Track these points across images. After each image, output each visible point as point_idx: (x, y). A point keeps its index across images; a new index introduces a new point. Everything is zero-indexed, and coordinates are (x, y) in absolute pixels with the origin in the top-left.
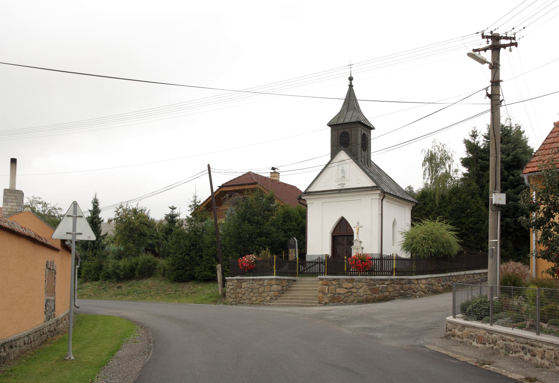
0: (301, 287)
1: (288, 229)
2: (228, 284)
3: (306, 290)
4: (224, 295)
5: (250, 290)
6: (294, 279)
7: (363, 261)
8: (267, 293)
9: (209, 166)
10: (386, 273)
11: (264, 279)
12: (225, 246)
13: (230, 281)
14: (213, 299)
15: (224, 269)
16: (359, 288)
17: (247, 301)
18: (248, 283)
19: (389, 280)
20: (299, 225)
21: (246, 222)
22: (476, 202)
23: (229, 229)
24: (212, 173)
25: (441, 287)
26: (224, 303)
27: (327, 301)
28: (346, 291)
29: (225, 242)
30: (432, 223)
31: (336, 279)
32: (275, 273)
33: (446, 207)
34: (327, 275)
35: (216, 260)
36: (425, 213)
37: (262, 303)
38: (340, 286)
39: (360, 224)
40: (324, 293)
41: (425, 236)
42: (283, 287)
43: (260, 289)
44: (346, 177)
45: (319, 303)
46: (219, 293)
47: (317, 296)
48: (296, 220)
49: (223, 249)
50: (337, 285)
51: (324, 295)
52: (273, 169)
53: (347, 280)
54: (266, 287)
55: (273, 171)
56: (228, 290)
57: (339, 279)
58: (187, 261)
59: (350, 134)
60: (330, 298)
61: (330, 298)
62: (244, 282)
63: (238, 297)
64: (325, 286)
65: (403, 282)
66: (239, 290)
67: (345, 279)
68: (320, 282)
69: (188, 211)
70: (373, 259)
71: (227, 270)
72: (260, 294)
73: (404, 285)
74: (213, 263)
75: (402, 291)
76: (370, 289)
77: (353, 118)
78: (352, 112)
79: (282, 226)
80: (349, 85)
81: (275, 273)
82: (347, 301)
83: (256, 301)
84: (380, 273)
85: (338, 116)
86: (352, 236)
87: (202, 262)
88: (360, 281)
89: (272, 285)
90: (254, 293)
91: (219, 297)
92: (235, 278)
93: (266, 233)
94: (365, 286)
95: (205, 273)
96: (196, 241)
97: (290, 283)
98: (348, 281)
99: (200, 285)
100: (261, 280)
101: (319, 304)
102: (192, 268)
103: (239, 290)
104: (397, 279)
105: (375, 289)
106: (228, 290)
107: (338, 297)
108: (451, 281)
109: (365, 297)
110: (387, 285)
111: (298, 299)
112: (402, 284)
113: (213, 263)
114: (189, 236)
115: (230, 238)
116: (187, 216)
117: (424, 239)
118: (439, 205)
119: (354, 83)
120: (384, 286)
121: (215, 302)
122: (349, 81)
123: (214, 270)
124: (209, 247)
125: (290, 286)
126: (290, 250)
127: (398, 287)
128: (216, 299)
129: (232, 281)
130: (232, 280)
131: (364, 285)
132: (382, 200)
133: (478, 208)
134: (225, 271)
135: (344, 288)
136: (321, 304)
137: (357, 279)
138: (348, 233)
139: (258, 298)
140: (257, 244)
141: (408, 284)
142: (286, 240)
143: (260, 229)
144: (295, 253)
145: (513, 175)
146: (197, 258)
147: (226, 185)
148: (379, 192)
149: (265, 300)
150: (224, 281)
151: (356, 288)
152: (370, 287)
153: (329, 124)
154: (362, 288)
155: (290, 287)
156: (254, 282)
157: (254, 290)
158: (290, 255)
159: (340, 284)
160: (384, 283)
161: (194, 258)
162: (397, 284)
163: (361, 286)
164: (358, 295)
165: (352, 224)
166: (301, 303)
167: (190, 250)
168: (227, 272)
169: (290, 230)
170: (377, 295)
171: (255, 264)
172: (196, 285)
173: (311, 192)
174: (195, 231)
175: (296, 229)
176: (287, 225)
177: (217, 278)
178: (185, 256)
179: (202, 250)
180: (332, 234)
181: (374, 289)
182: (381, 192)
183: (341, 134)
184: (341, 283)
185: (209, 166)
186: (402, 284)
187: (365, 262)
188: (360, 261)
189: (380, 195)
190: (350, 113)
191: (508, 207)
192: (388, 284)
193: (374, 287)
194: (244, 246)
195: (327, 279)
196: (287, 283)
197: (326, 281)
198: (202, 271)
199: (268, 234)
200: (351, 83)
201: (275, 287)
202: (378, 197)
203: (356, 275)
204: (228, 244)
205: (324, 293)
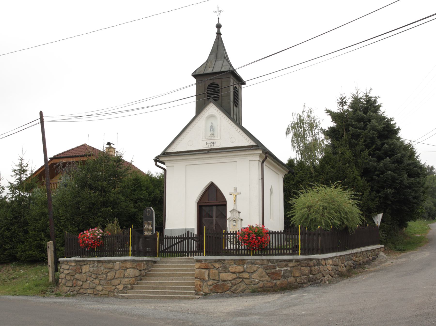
0: (165, 271)
1: (138, 199)
2: (62, 267)
3: (173, 275)
4: (56, 282)
5: (93, 276)
6: (154, 260)
8: (120, 279)
9: (41, 113)
11: (115, 261)
12: (58, 219)
13: (66, 263)
14: (40, 288)
15: (57, 247)
16: (252, 273)
17: (89, 291)
18: (91, 266)
19: (294, 261)
20: (150, 195)
21: (87, 189)
22: (352, 171)
23: (64, 198)
24: (45, 123)
25: (345, 269)
26: (56, 294)
27: (207, 290)
28: (234, 276)
29: (59, 213)
31: (219, 260)
32: (130, 253)
33: (317, 177)
34: (207, 254)
35: (46, 236)
36: (294, 183)
37: (112, 293)
38: (226, 270)
39: (238, 191)
41: (325, 204)
42: (140, 271)
43: (109, 274)
44: (216, 134)
45: (197, 294)
46: (48, 280)
47: (193, 284)
48: (147, 188)
49: (56, 222)
50: (221, 269)
51: (204, 283)
52: (109, 144)
53: (235, 261)
54: (118, 272)
55: (108, 146)
56: (62, 276)
57: (224, 260)
58: (7, 237)
61: (211, 287)
62: (85, 265)
63: (77, 285)
64: (204, 270)
65: (311, 263)
66: (77, 276)
67: (232, 260)
68: (198, 265)
69: (12, 176)
71: (59, 248)
72: (109, 282)
73: (313, 268)
74: (41, 240)
75: (311, 276)
78: (222, 61)
79: (131, 195)
80: (216, 33)
81: (130, 253)
82: (236, 290)
83: (102, 290)
84: (278, 252)
85: (205, 65)
86: (224, 205)
87: (27, 238)
88: (253, 263)
90: (100, 280)
91: (48, 285)
92: (72, 259)
93: (112, 202)
94: (260, 270)
95: (30, 252)
96: (20, 213)
97: (150, 266)
98: (237, 263)
99: (23, 268)
100: (110, 261)
102: (14, 246)
103: (77, 276)
104: (305, 259)
105: (275, 273)
106: (62, 276)
107: (223, 284)
108: (351, 260)
109: (261, 284)
110: (291, 267)
112: (310, 266)
113: (41, 240)
114: (11, 206)
115: (66, 208)
116: (10, 183)
117: (325, 208)
119: (222, 30)
120: (287, 269)
121: (43, 293)
123: (42, 249)
124: (37, 220)
125: (150, 269)
126: (146, 223)
127: (306, 270)
128: (45, 288)
129: (69, 264)
130: (68, 262)
131: (259, 268)
133: (355, 177)
134: (58, 250)
135: (231, 272)
136: (198, 295)
137: (249, 260)
138: (219, 202)
139: (105, 286)
140: (100, 216)
142: (136, 212)
143: (104, 197)
144: (152, 226)
145: (387, 143)
146: (20, 234)
147: (58, 156)
149: (116, 290)
150: (57, 263)
152: (268, 271)
153: (194, 74)
154: (257, 273)
155: (149, 271)
156: (100, 265)
157: (101, 276)
158: (145, 229)
159: (225, 267)
160: (288, 265)
161: (17, 234)
162: (305, 266)
163: (255, 269)
165: (226, 191)
166: (170, 293)
167: (11, 224)
168: (60, 251)
169: (140, 200)
170: (278, 282)
171: (102, 241)
172: (18, 268)
173: (171, 153)
174: (20, 200)
175: (147, 199)
176: (137, 195)
177: (47, 259)
178: (4, 231)
179: (27, 224)
181: (273, 273)
182: (263, 152)
183: (209, 85)
184: (227, 266)
185: (41, 113)
186: (310, 266)
187: (262, 236)
188: (255, 235)
189: (260, 156)
191: (386, 178)
192: (293, 267)
194: (83, 218)
195: (207, 260)
196: (146, 266)
197: (205, 264)
198: (27, 250)
199: (114, 204)
200: (219, 31)
201: (131, 272)
202: (258, 159)
203: (247, 255)
204: (62, 216)
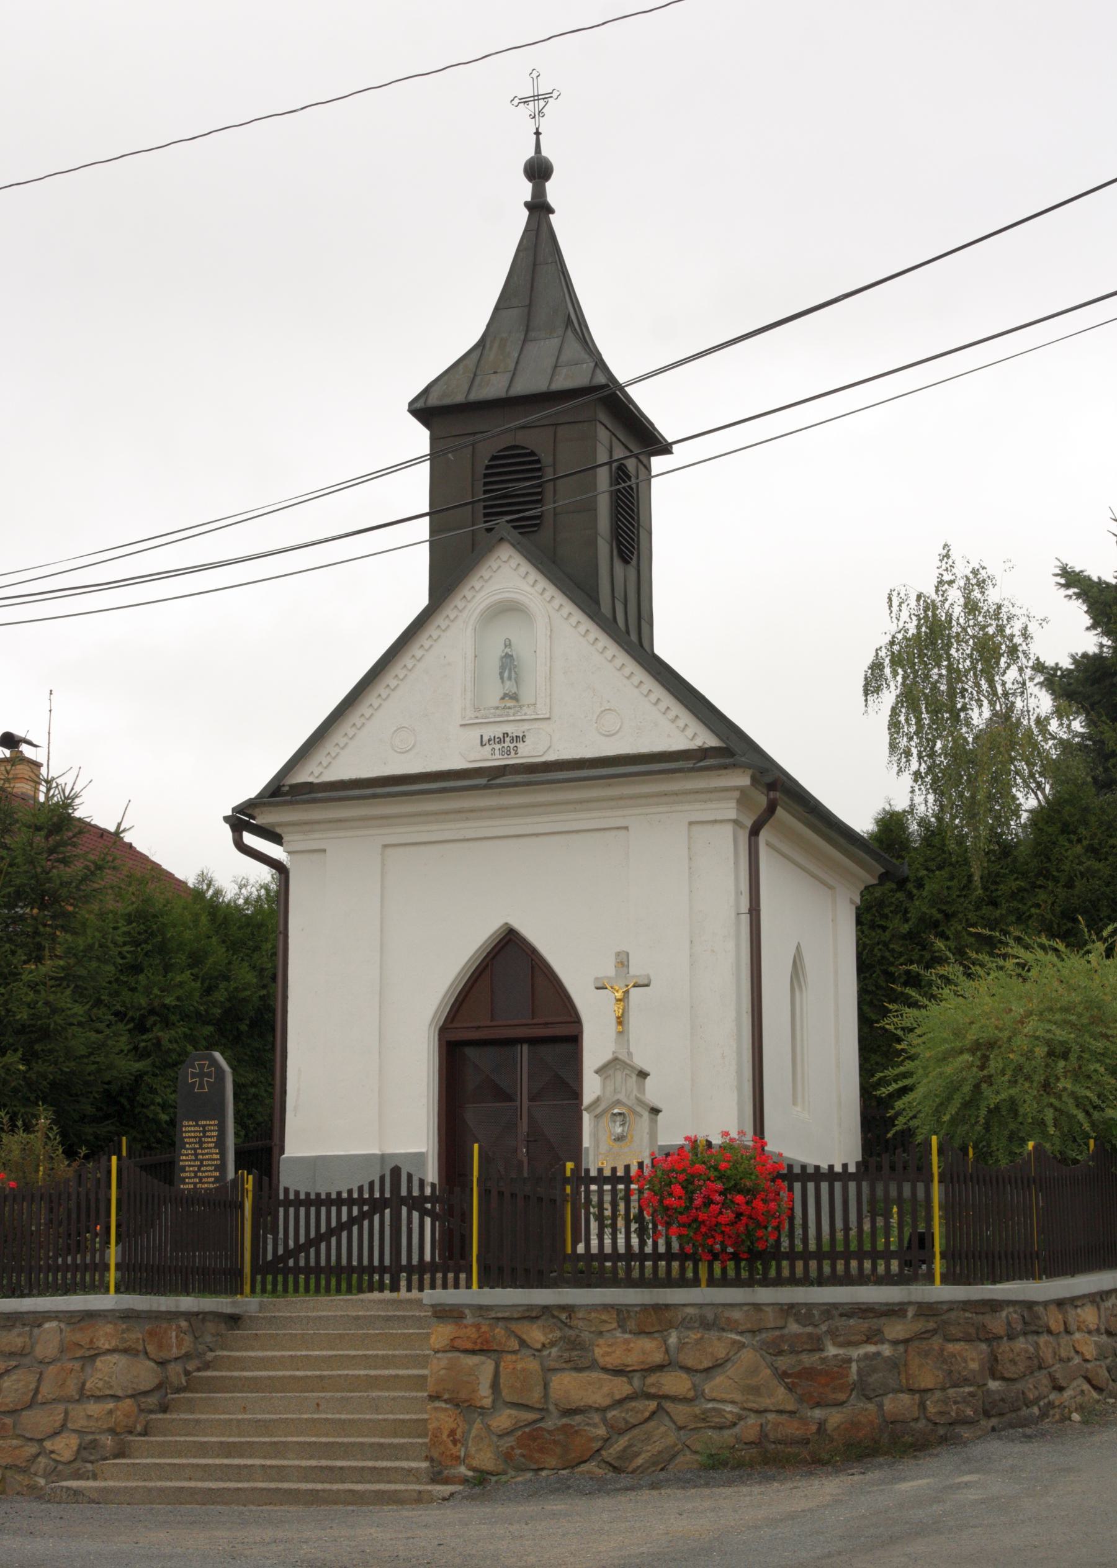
0: (281, 1363)
1: (152, 1012)
3: (320, 1383)
6: (229, 1310)
7: (737, 1188)
8: (61, 1408)
10: (854, 1264)
11: (37, 1319)
16: (707, 1370)
20: (209, 991)
27: (485, 1459)
28: (621, 1387)
30: (1075, 961)
31: (546, 1309)
33: (1022, 900)
36: (905, 928)
37: (19, 1477)
39: (636, 969)
40: (465, 1406)
42: (162, 1363)
44: (526, 697)
45: (437, 1477)
47: (419, 1427)
48: (196, 959)
50: (554, 1351)
51: (471, 1423)
53: (621, 1312)
54: (52, 1370)
57: (569, 1309)
59: (546, 459)
60: (510, 1441)
61: (510, 1441)
64: (471, 1360)
65: (997, 1324)
67: (606, 1307)
68: (441, 1334)
70: (797, 1178)
73: (1005, 1346)
75: (993, 1385)
76: (785, 1374)
77: (564, 371)
78: (555, 342)
79: (117, 993)
80: (527, 205)
82: (627, 1455)
84: (833, 1267)
89: (93, 1358)
93: (22, 1030)
94: (747, 1356)
97: (208, 1339)
98: (632, 1324)
101: (434, 1481)
109: (750, 1427)
110: (895, 1343)
111: (278, 1449)
112: (992, 1339)
118: (985, 889)
119: (553, 190)
120: (878, 1354)
122: (529, 186)
125: (210, 1356)
126: (189, 1130)
127: (972, 1357)
131: (743, 1346)
132: (755, 832)
135: (605, 1370)
136: (446, 1481)
141: (1022, 1339)
142: (139, 1077)
144: (221, 1143)
148: (742, 780)
149: (42, 1460)
151: (687, 1370)
152: (783, 1363)
153: (419, 405)
154: (731, 1370)
155: (207, 1366)
159: (574, 1344)
160: (879, 1332)
162: (968, 1339)
163: (721, 1353)
164: (704, 1417)
166: (307, 1474)
169: (163, 1015)
170: (835, 1418)
173: (310, 787)
180: (443, 1031)
181: (808, 1373)
182: (754, 779)
183: (494, 458)
184: (586, 1336)
186: (992, 1339)
187: (752, 1192)
188: (719, 1185)
189: (744, 800)
190: (543, 350)
192: (906, 1341)
193: (809, 1360)
195: (489, 1308)
196: (188, 1340)
197: (478, 1327)
200: (539, 192)
202: (732, 814)
205: (465, 1406)
